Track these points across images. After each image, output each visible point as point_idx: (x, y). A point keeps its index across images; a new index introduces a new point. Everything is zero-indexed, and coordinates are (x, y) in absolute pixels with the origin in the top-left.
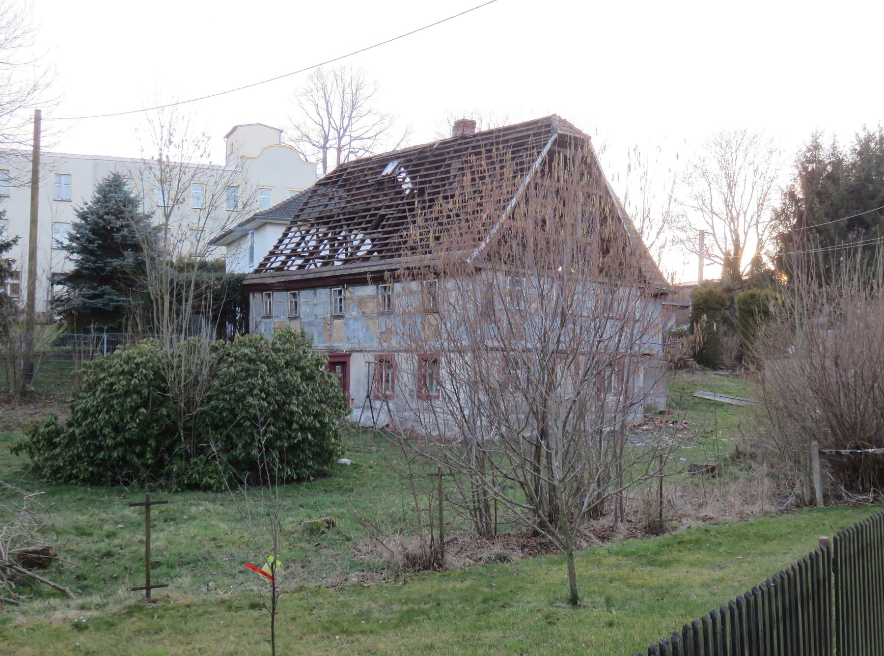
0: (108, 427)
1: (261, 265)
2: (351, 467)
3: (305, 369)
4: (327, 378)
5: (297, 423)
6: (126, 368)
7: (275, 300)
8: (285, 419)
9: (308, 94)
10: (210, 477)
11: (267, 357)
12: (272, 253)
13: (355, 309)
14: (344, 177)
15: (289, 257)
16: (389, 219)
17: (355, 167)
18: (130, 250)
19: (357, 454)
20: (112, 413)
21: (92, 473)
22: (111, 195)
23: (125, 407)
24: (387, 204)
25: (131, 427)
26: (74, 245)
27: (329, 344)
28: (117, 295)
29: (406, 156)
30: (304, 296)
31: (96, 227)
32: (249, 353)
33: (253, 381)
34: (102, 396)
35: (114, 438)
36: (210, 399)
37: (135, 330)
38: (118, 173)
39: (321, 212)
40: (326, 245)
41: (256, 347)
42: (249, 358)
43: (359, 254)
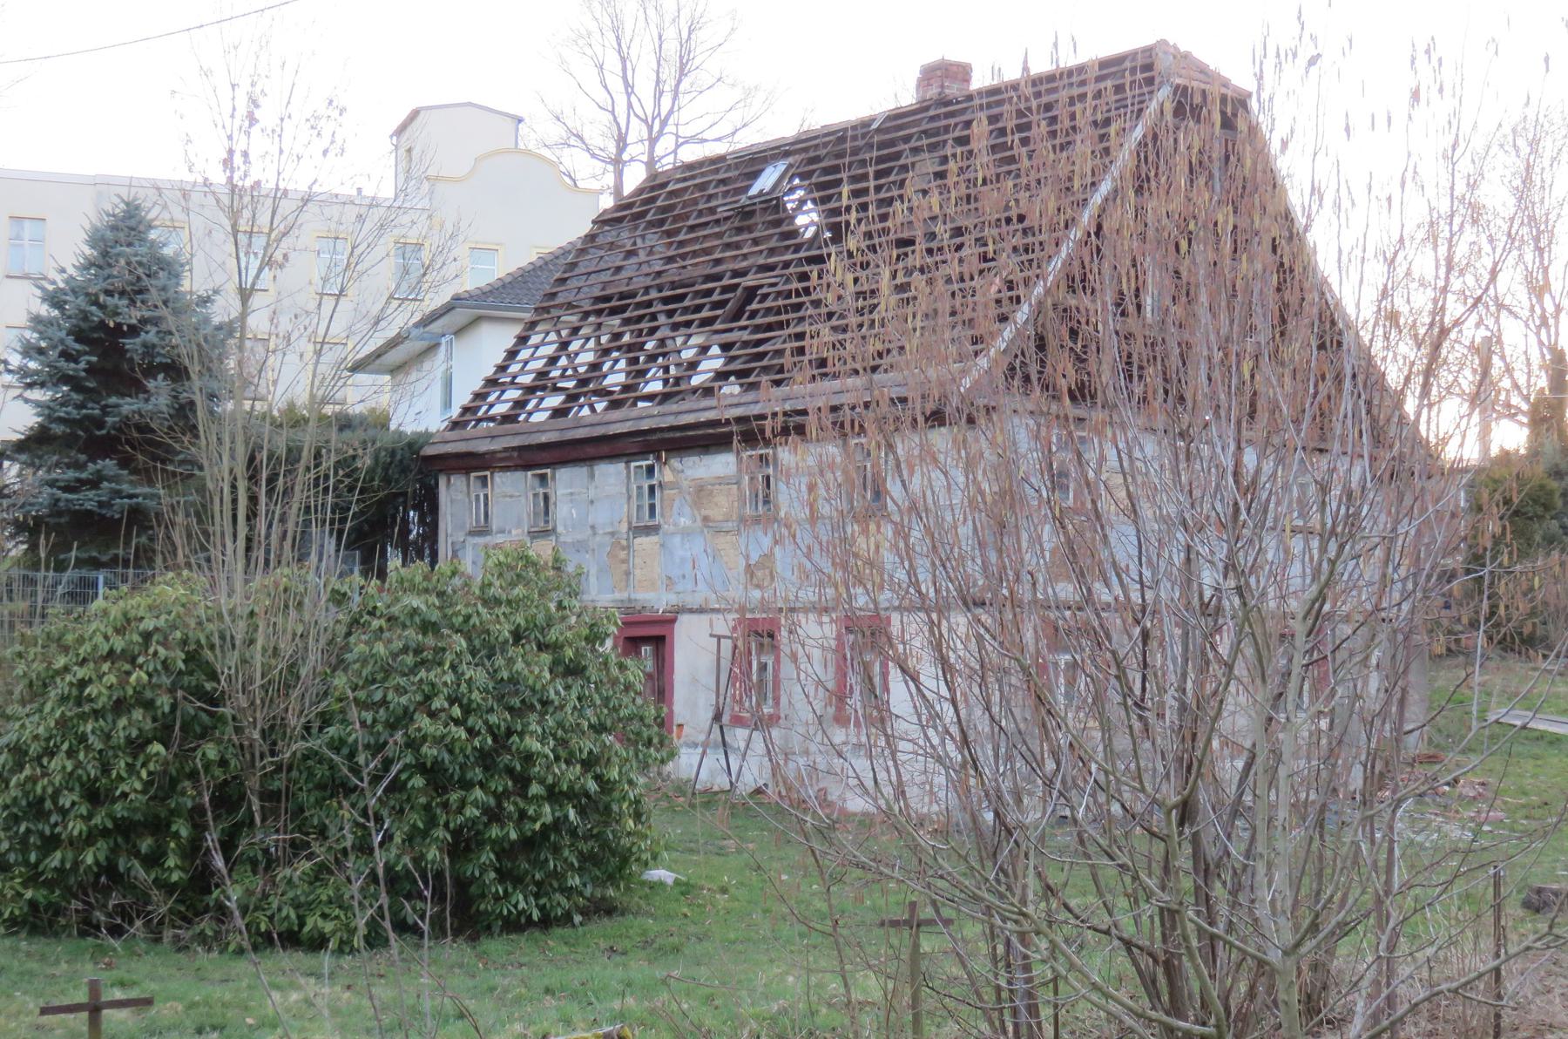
0: (71, 790)
1: (466, 410)
2: (677, 890)
3: (562, 647)
4: (615, 671)
5: (542, 782)
6: (119, 644)
7: (497, 490)
8: (510, 771)
9: (581, 42)
10: (324, 916)
11: (467, 618)
12: (492, 382)
13: (687, 510)
14: (659, 203)
15: (530, 390)
16: (765, 297)
17: (685, 179)
18: (161, 376)
19: (688, 857)
20: (81, 756)
21: (33, 904)
22: (119, 249)
23: (114, 742)
24: (761, 261)
25: (127, 789)
26: (33, 365)
27: (625, 595)
28: (131, 482)
29: (805, 150)
30: (566, 480)
31: (84, 325)
32: (423, 607)
33: (432, 675)
34: (58, 714)
35: (87, 818)
36: (326, 719)
37: (170, 562)
38: (135, 199)
39: (605, 285)
40: (616, 361)
41: (441, 594)
42: (423, 621)
43: (696, 381)
